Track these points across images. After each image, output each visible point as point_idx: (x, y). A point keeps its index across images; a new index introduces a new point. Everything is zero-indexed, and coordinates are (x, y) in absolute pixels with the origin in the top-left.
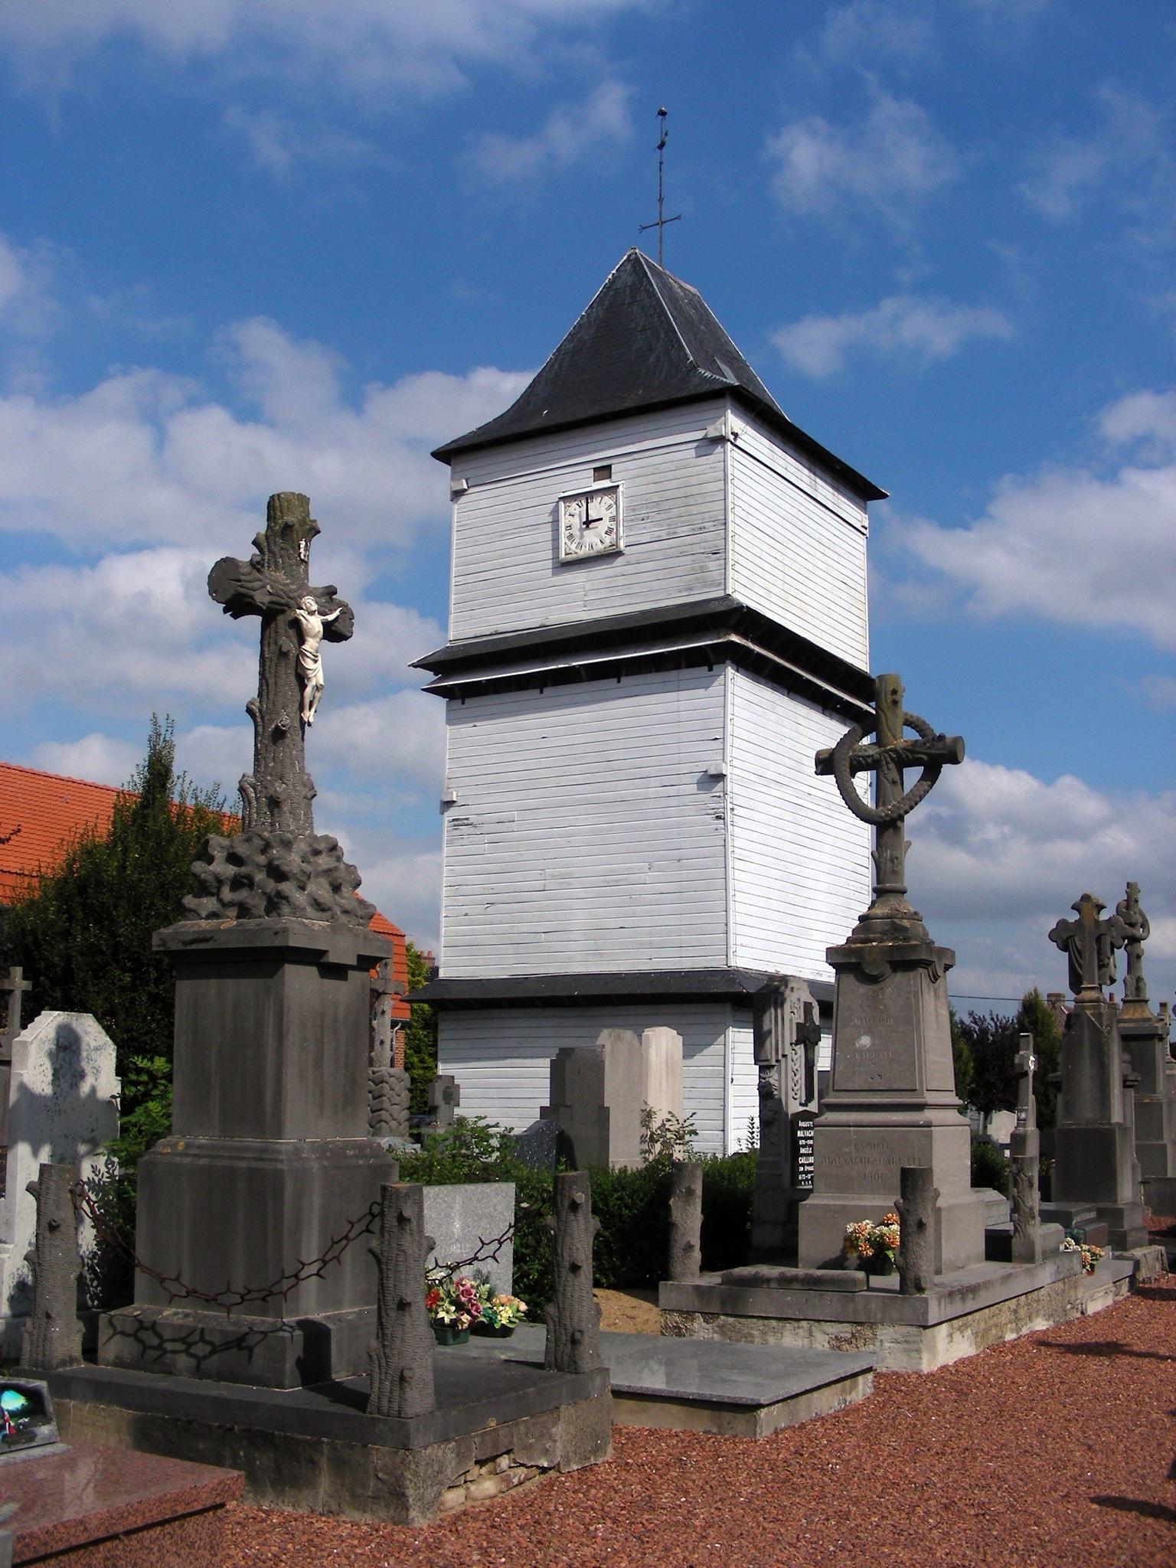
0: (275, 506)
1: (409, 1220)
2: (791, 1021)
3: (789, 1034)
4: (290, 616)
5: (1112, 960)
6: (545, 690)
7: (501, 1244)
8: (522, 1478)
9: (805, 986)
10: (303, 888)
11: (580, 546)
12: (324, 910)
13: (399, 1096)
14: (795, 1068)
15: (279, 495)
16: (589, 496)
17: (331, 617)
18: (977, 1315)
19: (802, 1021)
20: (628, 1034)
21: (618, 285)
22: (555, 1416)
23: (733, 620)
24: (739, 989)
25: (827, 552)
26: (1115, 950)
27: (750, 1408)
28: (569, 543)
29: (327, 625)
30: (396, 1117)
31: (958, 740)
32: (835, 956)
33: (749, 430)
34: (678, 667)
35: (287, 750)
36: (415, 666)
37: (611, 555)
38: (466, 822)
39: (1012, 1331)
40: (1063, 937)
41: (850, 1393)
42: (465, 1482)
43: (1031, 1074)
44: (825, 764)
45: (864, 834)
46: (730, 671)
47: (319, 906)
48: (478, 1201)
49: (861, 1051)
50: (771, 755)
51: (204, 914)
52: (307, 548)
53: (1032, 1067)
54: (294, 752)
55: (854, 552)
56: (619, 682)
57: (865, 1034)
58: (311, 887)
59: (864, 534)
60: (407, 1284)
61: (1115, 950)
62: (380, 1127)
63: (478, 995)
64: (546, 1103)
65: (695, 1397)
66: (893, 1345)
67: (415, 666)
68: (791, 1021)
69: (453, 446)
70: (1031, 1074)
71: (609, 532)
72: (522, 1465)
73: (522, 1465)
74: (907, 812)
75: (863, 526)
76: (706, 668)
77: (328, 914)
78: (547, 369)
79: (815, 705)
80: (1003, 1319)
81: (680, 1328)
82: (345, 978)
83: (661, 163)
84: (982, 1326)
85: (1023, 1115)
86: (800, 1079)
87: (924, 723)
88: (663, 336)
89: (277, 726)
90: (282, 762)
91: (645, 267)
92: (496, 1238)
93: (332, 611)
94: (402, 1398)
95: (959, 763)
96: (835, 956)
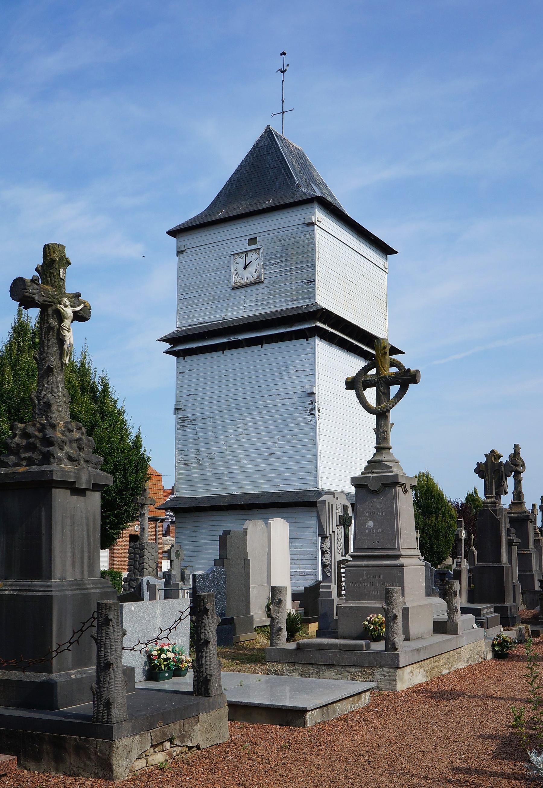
0: (48, 250)
1: (111, 620)
2: (336, 514)
3: (335, 521)
4: (55, 307)
5: (505, 483)
7: (170, 630)
8: (178, 752)
9: (344, 496)
10: (62, 450)
11: (242, 278)
12: (74, 461)
13: (153, 555)
14: (339, 538)
15: (48, 245)
16: (246, 253)
17: (77, 309)
18: (427, 661)
19: (342, 514)
20: (260, 523)
22: (196, 719)
26: (507, 477)
27: (303, 712)
29: (75, 313)
30: (151, 566)
31: (417, 371)
32: (355, 481)
33: (326, 218)
34: (291, 339)
35: (54, 378)
37: (257, 282)
38: (187, 419)
39: (446, 669)
40: (480, 470)
41: (357, 703)
42: (146, 756)
43: (463, 540)
44: (351, 384)
45: (373, 418)
47: (71, 459)
48: (170, 608)
49: (368, 529)
50: (329, 394)
51: (11, 464)
52: (64, 272)
53: (464, 536)
54: (58, 379)
55: (381, 281)
57: (370, 520)
58: (67, 448)
59: (386, 272)
60: (111, 654)
61: (507, 477)
62: (144, 571)
64: (218, 558)
65: (274, 707)
66: (382, 677)
68: (336, 514)
69: (177, 228)
70: (463, 540)
71: (256, 271)
72: (178, 746)
73: (178, 746)
74: (391, 408)
75: (385, 268)
77: (77, 462)
78: (225, 188)
80: (441, 663)
81: (276, 671)
82: (84, 495)
83: (283, 80)
84: (430, 667)
85: (459, 560)
86: (342, 543)
87: (400, 363)
88: (283, 171)
89: (49, 366)
90: (52, 384)
91: (274, 135)
92: (168, 628)
93: (79, 305)
94: (109, 714)
95: (418, 383)
96: (355, 481)
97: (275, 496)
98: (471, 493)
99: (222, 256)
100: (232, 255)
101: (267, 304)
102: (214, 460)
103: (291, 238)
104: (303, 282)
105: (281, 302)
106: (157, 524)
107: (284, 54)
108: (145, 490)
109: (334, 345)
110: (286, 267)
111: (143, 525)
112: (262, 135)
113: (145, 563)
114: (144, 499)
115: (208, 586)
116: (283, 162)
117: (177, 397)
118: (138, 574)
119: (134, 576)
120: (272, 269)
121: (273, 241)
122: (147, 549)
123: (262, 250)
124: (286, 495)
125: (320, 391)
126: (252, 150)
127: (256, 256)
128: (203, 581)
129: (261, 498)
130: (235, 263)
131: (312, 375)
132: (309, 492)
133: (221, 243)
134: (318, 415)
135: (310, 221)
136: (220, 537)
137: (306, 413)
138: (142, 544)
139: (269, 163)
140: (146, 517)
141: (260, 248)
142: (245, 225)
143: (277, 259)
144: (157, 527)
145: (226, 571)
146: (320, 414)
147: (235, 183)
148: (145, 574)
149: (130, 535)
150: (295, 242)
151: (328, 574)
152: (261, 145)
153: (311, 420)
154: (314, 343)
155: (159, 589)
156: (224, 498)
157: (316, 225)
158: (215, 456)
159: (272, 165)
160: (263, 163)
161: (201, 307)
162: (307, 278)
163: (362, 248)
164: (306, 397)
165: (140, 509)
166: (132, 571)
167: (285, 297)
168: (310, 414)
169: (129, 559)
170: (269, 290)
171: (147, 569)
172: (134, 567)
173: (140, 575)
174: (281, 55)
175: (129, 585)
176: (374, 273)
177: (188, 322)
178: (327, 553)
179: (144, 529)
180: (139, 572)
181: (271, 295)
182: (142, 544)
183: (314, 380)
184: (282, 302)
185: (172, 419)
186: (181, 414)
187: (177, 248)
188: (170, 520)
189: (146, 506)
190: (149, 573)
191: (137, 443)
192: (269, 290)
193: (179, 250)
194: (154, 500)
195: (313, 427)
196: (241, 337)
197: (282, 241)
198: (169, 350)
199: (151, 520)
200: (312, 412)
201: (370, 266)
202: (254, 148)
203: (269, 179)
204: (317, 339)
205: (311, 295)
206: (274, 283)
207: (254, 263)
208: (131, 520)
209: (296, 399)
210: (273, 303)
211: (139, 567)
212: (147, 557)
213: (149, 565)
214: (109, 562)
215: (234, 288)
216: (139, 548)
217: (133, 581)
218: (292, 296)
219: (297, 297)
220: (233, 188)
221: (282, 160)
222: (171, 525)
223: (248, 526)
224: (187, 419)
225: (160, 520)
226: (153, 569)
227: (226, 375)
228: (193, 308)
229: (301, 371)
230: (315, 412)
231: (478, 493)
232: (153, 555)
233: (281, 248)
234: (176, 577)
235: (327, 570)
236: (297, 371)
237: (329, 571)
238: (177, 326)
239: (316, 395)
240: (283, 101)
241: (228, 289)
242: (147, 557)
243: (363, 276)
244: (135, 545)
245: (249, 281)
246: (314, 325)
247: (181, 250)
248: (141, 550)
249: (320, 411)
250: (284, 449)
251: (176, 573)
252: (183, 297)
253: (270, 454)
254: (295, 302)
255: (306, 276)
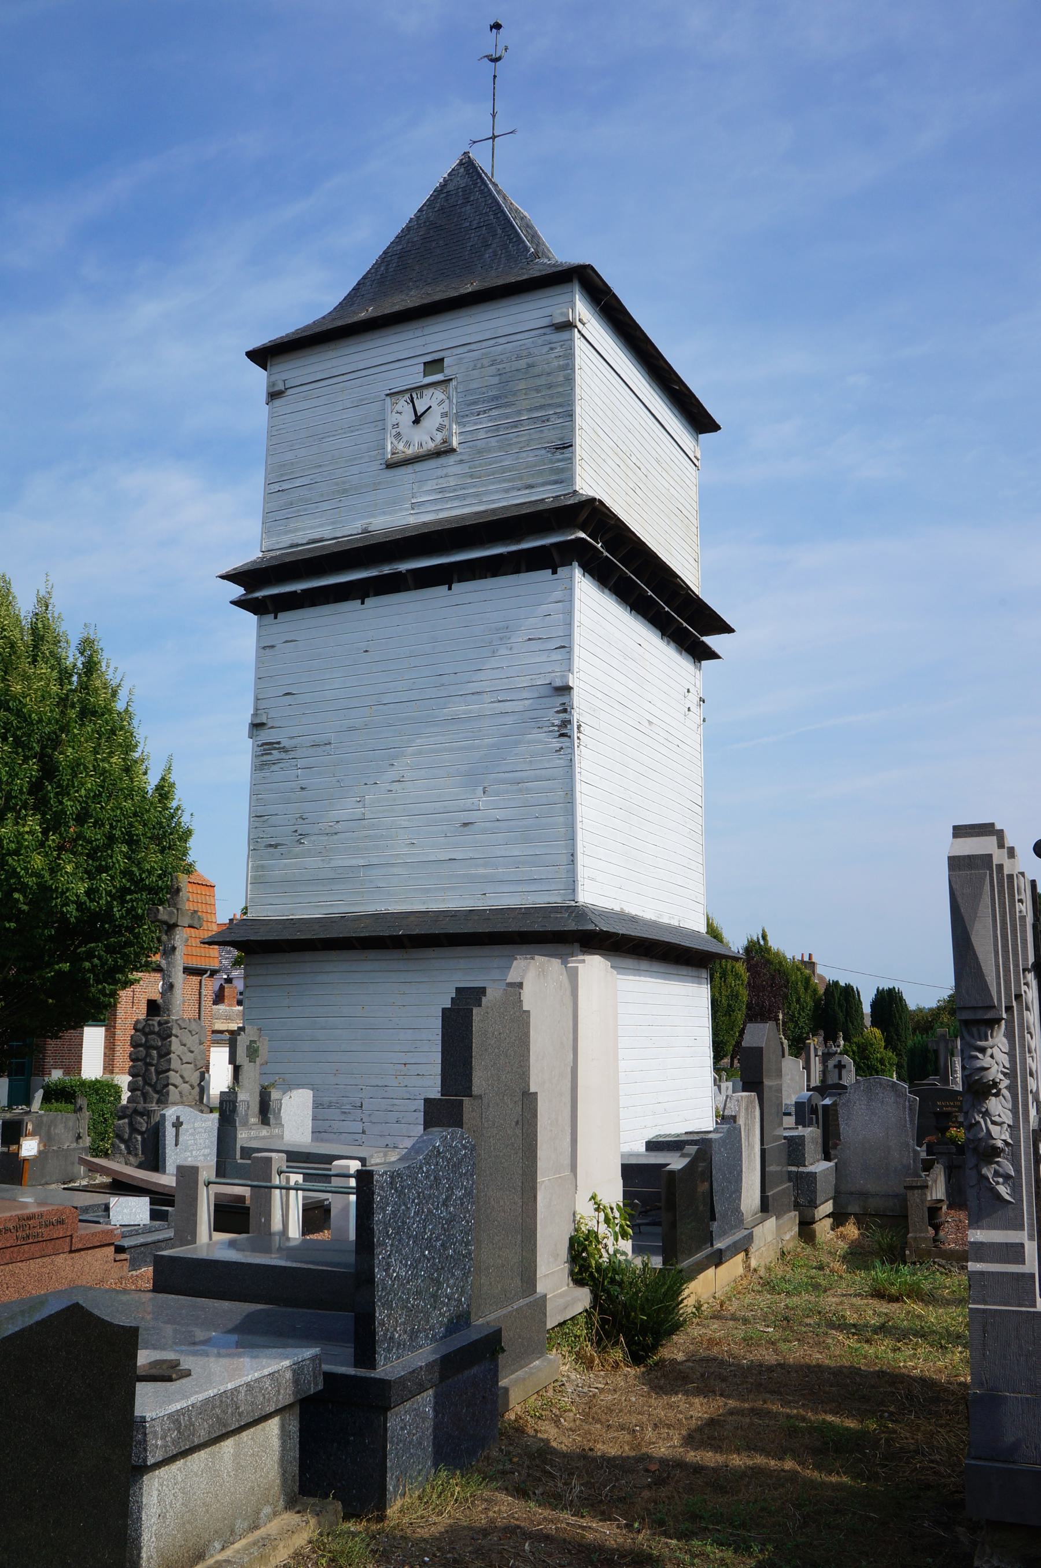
6: (367, 600)
11: (408, 444)
13: (192, 1052)
21: (450, 187)
23: (583, 516)
24: (591, 927)
25: (664, 474)
28: (396, 442)
30: (187, 1079)
34: (327, 602)
36: (223, 577)
37: (444, 451)
38: (277, 746)
46: (578, 573)
50: (599, 695)
56: (450, 589)
63: (287, 936)
64: (435, 1093)
67: (223, 577)
75: (695, 457)
76: (550, 571)
79: (655, 629)
83: (495, 77)
88: (499, 231)
97: (476, 918)
98: (755, 939)
99: (366, 399)
100: (387, 395)
101: (464, 497)
102: (335, 837)
103: (519, 358)
104: (545, 448)
105: (497, 491)
106: (203, 982)
107: (497, 26)
108: (178, 890)
109: (607, 591)
110: (507, 418)
111: (170, 977)
112: (453, 170)
113: (173, 1070)
114: (175, 911)
115: (417, 1213)
116: (499, 215)
117: (257, 699)
118: (153, 1097)
119: (145, 1102)
120: (476, 424)
121: (479, 366)
122: (177, 1036)
123: (454, 383)
124: (501, 916)
125: (582, 685)
126: (432, 198)
127: (442, 396)
128: (399, 1197)
129: (444, 922)
130: (394, 413)
131: (566, 648)
132: (556, 909)
133: (364, 373)
134: (578, 738)
135: (564, 319)
136: (447, 1015)
137: (550, 731)
138: (167, 1022)
139: (469, 220)
140: (180, 960)
141: (451, 379)
142: (418, 333)
143: (489, 402)
144: (203, 987)
145: (473, 1148)
146: (581, 736)
147: (396, 261)
148: (171, 1099)
149: (148, 1000)
150: (530, 366)
151: (1003, 1190)
152: (450, 187)
153: (562, 748)
154: (571, 578)
155: (209, 1183)
156: (357, 922)
157: (576, 330)
158: (339, 827)
159: (475, 222)
160: (456, 220)
161: (317, 507)
162: (554, 440)
163: (657, 405)
164: (550, 697)
165: (164, 938)
166: (139, 1090)
167: (505, 481)
168: (558, 733)
169: (132, 1060)
170: (470, 468)
171: (176, 1086)
172: (145, 1080)
173: (159, 1102)
174: (491, 30)
175: (131, 1124)
176: (676, 461)
177: (286, 540)
178: (997, 1095)
179: (171, 986)
180: (157, 1092)
181: (472, 477)
182: (167, 1022)
183: (569, 660)
184: (497, 492)
185: (245, 748)
186: (266, 736)
187: (268, 387)
188: (225, 977)
189: (178, 930)
190: (181, 1097)
191: (164, 791)
192: (470, 468)
193: (271, 390)
194: (199, 917)
195: (567, 763)
196: (404, 567)
197: (499, 363)
198: (243, 598)
199: (189, 971)
200: (564, 730)
201: (669, 445)
202: (435, 194)
203: (469, 248)
204: (577, 571)
205: (565, 474)
206: (479, 453)
207: (437, 411)
208: (144, 966)
209: (526, 702)
210: (476, 495)
211: (158, 1079)
212: (178, 1056)
213: (182, 1077)
214: (105, 1054)
215: (390, 466)
216: (158, 1034)
217: (142, 1114)
218: (521, 479)
219: (530, 481)
220: (392, 270)
221: (497, 211)
222: (226, 985)
223: (523, 977)
224: (277, 746)
225: (209, 972)
226: (191, 1086)
227: (367, 651)
228: (299, 511)
229: (540, 639)
230: (572, 729)
231: (769, 938)
232: (192, 1052)
233: (497, 378)
234: (248, 1108)
235: (997, 1174)
236: (530, 639)
237: (1007, 1177)
238: (261, 548)
239: (575, 692)
240: (494, 116)
241: (376, 466)
242: (178, 1056)
243: (658, 462)
244: (149, 1025)
245: (425, 449)
246: (573, 537)
247: (277, 389)
248: (164, 1039)
249: (582, 729)
250: (498, 814)
251: (247, 1098)
252: (276, 487)
253: (465, 825)
254: (527, 491)
255: (552, 436)
